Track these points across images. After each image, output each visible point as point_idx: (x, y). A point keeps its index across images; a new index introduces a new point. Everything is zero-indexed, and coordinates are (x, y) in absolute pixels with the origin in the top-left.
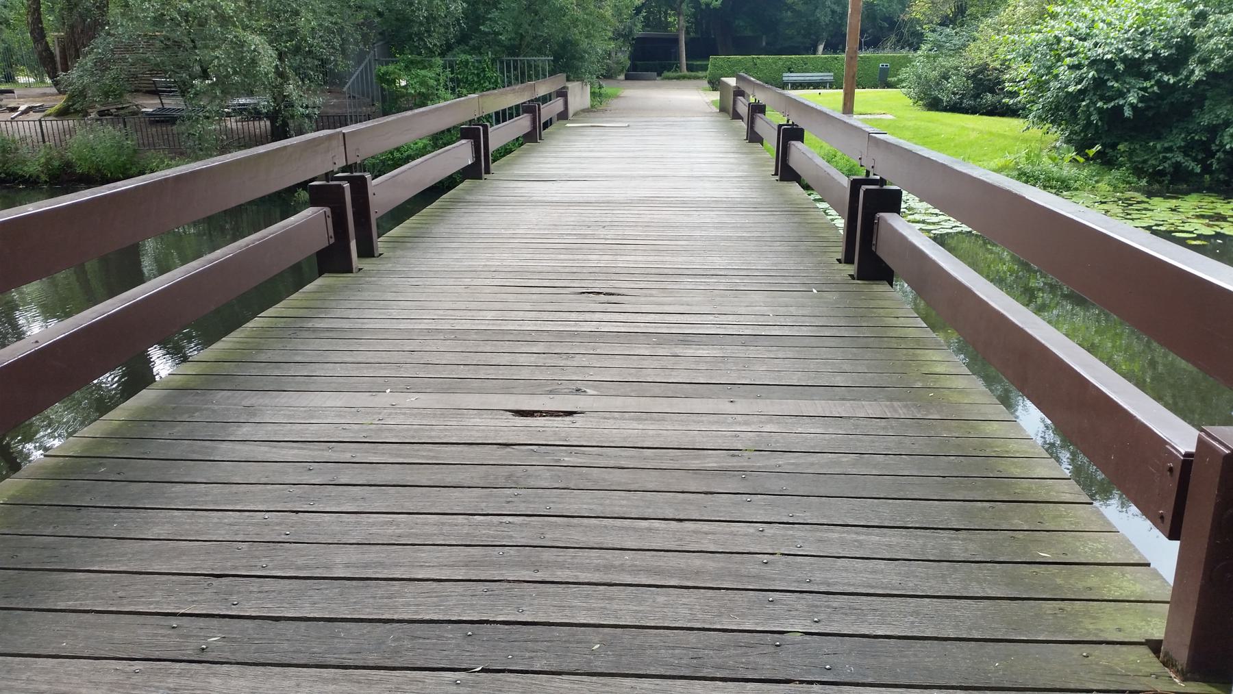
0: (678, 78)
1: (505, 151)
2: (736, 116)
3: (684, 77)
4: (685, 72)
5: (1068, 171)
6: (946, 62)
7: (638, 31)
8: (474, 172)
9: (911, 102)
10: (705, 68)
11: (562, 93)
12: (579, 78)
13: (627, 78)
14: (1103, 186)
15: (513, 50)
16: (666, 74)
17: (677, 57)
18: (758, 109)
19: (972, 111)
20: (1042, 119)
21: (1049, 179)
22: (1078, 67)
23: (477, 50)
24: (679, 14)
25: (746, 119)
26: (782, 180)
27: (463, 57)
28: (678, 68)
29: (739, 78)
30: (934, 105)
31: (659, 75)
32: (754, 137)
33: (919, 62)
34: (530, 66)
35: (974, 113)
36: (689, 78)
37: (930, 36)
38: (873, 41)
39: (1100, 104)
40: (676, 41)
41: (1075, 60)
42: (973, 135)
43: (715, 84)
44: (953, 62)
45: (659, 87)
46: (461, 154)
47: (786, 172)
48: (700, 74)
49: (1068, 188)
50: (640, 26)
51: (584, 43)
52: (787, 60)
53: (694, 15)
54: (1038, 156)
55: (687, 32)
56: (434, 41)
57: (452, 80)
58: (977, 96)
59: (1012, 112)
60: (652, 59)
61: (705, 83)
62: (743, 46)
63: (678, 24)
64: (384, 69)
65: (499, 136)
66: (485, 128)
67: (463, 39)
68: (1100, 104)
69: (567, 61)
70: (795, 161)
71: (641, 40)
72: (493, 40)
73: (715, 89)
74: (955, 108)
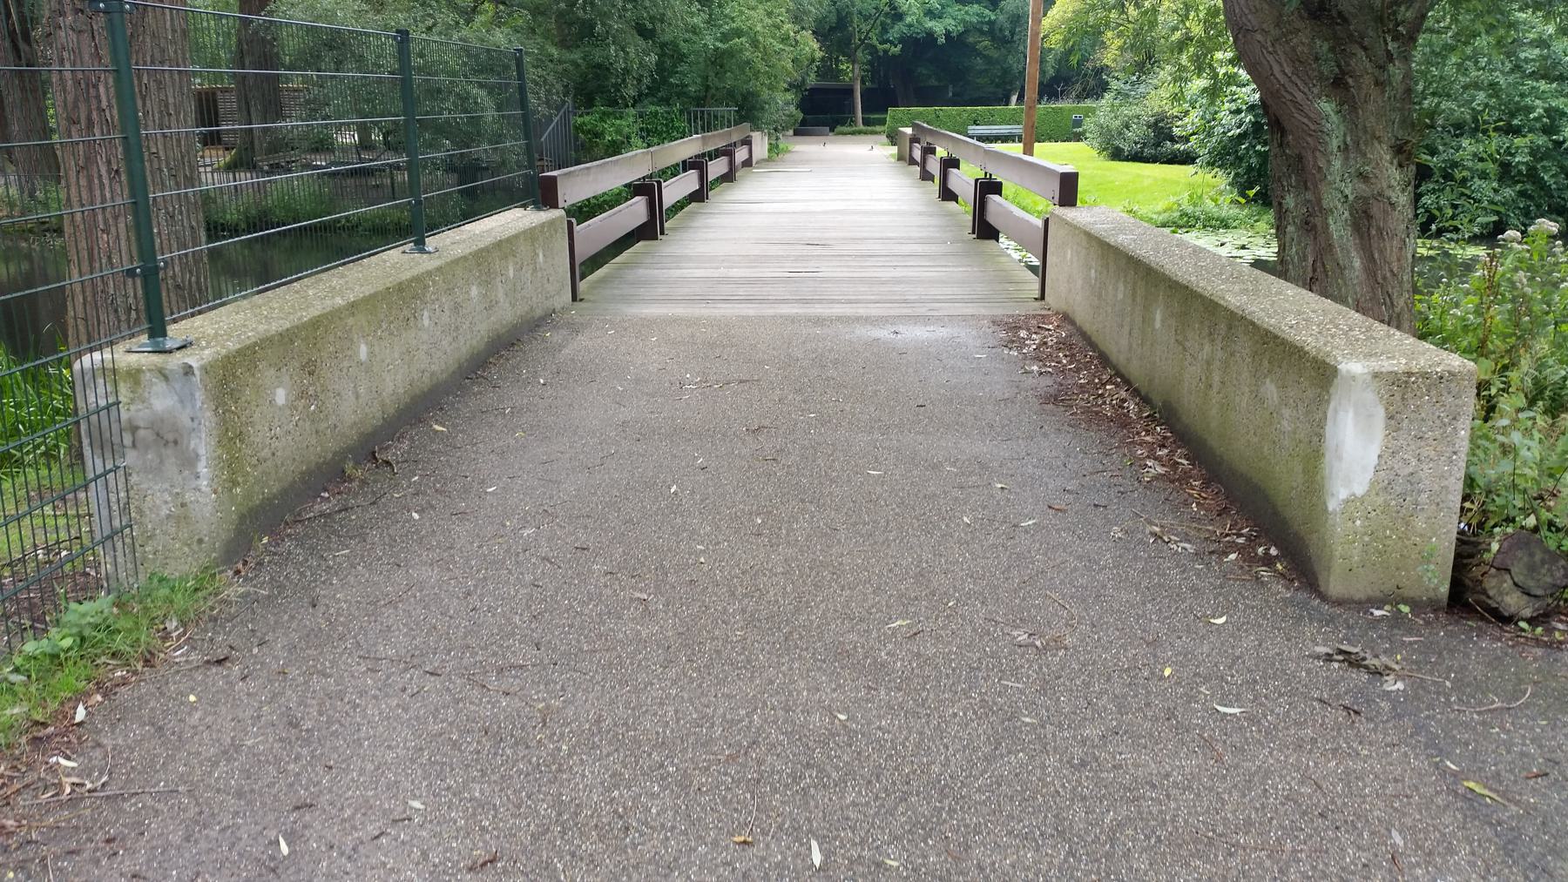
0: (853, 133)
1: (679, 206)
2: (912, 162)
3: (860, 132)
4: (861, 127)
5: (1228, 211)
6: (1127, 111)
7: (812, 80)
8: (648, 231)
9: (1095, 153)
10: (882, 122)
11: (747, 142)
12: (758, 129)
13: (796, 133)
14: (1262, 226)
15: (700, 101)
16: (839, 128)
17: (853, 111)
18: (951, 163)
19: (1153, 159)
20: (1211, 164)
21: (1210, 219)
22: (1238, 111)
23: (666, 101)
24: (853, 62)
25: (937, 180)
26: (978, 237)
27: (653, 108)
28: (853, 122)
29: (915, 126)
30: (1117, 155)
31: (832, 130)
32: (948, 195)
33: (1103, 111)
34: (716, 117)
35: (1154, 162)
36: (866, 133)
37: (1114, 85)
38: (1050, 90)
39: (1258, 147)
40: (849, 92)
41: (1233, 106)
42: (1146, 183)
43: (893, 138)
44: (1136, 110)
45: (832, 142)
46: (635, 212)
47: (985, 230)
48: (878, 128)
49: (1226, 227)
50: (813, 76)
51: (765, 94)
52: (973, 112)
53: (870, 63)
54: (1201, 197)
55: (863, 82)
56: (631, 91)
57: (642, 129)
58: (1157, 145)
59: (1187, 159)
60: (824, 111)
61: (884, 138)
62: (927, 97)
63: (851, 72)
64: (579, 120)
65: (674, 190)
66: (659, 184)
67: (653, 90)
68: (1258, 147)
69: (748, 111)
70: (992, 218)
71: (813, 91)
72: (681, 93)
73: (894, 144)
74: (1137, 157)
